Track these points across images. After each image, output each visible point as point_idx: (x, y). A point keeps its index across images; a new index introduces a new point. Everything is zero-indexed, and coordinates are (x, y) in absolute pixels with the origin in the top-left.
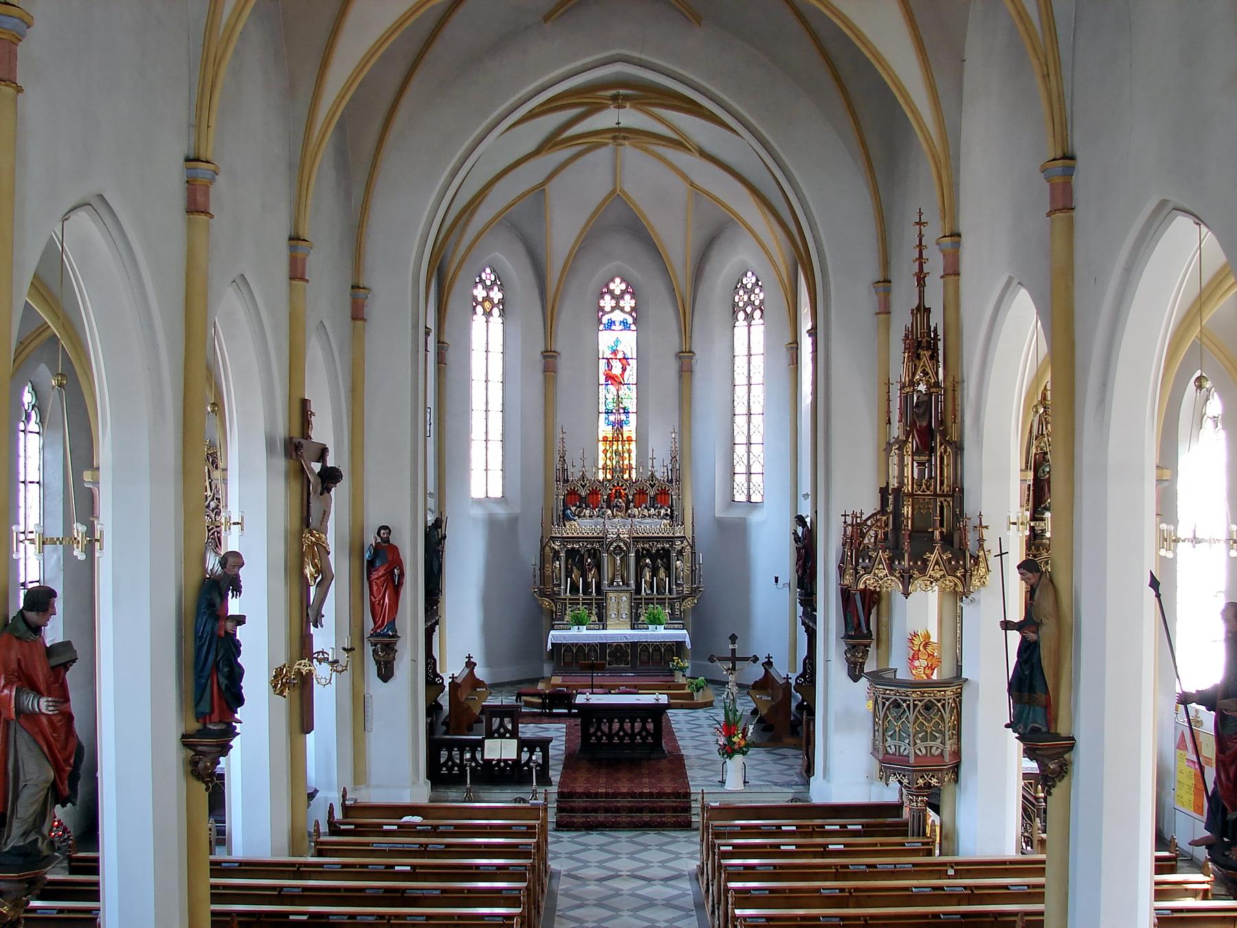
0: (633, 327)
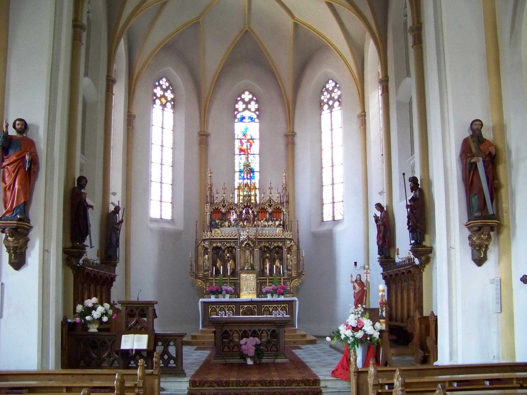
0: (257, 120)
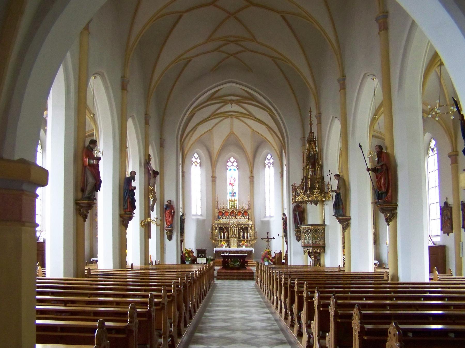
0: (237, 171)
